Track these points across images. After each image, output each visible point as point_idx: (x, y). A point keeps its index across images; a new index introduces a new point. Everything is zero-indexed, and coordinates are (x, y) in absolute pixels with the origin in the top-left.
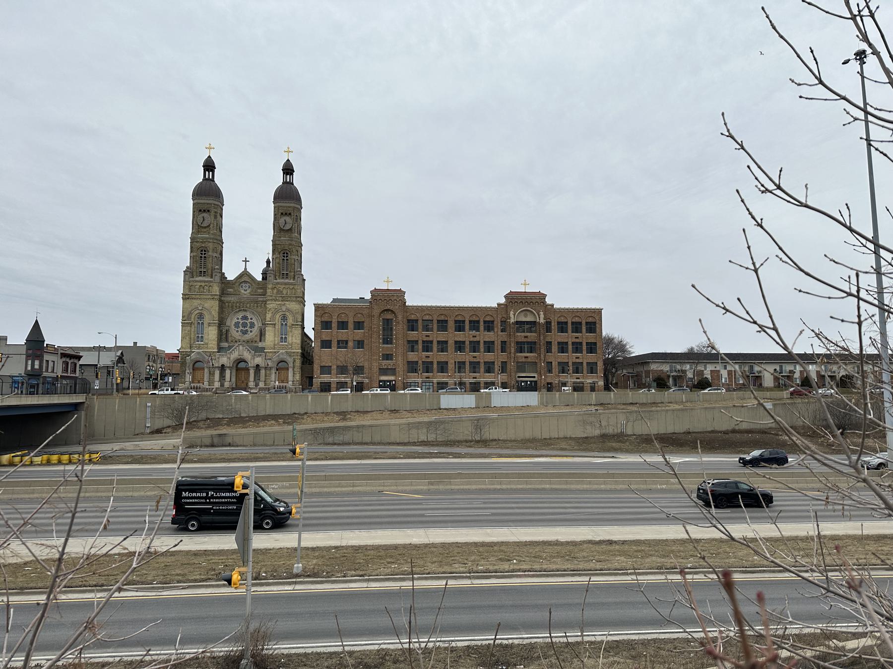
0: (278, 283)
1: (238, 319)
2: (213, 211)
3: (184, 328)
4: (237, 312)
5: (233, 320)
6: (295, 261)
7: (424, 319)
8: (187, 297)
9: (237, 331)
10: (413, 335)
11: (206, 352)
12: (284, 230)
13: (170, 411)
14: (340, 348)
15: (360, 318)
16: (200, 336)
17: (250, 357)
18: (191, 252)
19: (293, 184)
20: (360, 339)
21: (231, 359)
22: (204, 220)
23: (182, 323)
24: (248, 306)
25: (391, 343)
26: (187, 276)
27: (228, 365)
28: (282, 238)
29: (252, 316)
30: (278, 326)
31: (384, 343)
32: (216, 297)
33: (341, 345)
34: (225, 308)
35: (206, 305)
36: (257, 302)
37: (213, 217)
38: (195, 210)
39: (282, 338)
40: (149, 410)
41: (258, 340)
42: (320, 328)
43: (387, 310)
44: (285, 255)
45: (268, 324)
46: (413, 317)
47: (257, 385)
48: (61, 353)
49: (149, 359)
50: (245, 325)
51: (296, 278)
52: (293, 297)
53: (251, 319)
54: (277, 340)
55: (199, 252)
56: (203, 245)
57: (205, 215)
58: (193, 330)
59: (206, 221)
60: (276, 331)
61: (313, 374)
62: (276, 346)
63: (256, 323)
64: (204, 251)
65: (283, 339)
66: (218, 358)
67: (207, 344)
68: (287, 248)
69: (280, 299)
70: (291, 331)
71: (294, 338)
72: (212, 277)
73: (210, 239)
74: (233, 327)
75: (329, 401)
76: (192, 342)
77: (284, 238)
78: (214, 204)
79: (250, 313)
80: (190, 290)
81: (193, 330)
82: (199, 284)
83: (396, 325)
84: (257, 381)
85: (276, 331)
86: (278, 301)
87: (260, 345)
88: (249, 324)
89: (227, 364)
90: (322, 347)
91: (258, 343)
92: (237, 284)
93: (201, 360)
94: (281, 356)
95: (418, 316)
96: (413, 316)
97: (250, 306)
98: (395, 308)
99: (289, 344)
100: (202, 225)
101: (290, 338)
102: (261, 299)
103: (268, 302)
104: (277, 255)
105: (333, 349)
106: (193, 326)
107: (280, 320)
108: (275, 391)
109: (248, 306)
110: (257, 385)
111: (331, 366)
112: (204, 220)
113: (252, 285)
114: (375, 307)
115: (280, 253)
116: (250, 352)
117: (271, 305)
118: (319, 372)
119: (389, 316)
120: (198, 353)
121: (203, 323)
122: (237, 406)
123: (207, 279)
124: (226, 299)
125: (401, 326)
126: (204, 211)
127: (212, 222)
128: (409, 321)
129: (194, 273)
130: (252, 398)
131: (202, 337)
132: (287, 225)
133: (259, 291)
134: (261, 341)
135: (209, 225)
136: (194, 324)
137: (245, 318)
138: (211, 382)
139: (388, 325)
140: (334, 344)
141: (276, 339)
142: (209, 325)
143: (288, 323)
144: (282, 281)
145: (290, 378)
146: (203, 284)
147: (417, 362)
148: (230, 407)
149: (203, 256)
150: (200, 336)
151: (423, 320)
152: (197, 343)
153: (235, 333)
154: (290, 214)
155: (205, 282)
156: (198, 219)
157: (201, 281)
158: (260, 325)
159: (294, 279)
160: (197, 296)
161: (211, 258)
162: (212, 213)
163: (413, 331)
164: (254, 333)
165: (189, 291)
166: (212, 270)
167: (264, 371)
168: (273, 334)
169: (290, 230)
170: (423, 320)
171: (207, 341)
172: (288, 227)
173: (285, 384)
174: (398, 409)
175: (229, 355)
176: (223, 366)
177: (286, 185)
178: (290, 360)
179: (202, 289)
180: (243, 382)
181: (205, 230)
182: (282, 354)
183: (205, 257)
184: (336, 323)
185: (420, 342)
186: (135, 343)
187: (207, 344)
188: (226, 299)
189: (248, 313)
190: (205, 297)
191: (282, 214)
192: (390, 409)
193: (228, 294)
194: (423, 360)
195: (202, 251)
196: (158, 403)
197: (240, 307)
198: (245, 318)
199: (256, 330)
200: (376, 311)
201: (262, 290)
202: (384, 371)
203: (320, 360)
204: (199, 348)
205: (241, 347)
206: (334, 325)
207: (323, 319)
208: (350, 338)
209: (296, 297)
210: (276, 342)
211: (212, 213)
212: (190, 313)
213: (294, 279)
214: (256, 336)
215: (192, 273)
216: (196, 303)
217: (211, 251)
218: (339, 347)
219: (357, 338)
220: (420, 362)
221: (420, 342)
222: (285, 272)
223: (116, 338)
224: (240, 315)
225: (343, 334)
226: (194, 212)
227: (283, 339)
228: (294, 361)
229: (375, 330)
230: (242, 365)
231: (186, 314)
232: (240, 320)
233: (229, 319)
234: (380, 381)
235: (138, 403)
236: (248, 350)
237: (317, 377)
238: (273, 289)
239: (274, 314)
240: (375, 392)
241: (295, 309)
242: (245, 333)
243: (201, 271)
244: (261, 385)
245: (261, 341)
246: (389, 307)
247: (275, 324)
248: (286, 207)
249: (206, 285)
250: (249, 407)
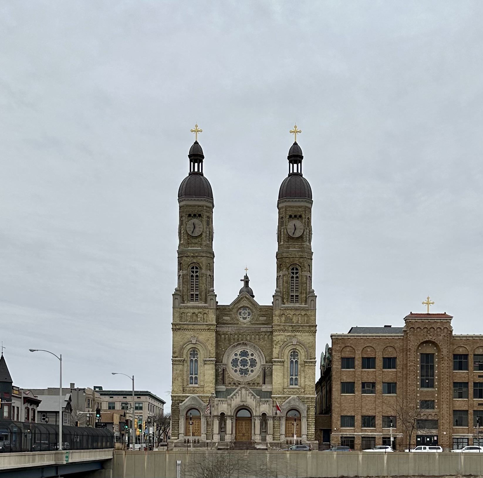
0: (287, 309)
1: (236, 355)
3: (175, 367)
4: (234, 346)
5: (228, 359)
6: (306, 279)
7: (476, 353)
8: (177, 327)
9: (252, 371)
10: (461, 375)
11: (202, 397)
12: (293, 238)
13: (200, 470)
14: (365, 393)
15: (390, 353)
16: (194, 376)
17: (255, 403)
18: (180, 269)
19: (202, 175)
20: (390, 381)
21: (232, 405)
22: (194, 228)
23: (173, 361)
24: (248, 338)
25: (432, 386)
27: (229, 414)
30: (287, 364)
31: (422, 386)
32: (212, 327)
33: (366, 388)
36: (259, 333)
37: (205, 223)
39: (292, 379)
40: (179, 468)
41: (261, 381)
42: (340, 367)
43: (426, 342)
44: (295, 271)
45: (275, 361)
46: (461, 351)
47: (264, 439)
48: (24, 397)
49: (89, 404)
50: (244, 363)
51: (209, 299)
52: (306, 326)
53: (252, 355)
54: (287, 381)
55: (190, 269)
56: (195, 261)
57: (196, 221)
59: (197, 229)
60: (285, 371)
61: (331, 426)
62: (285, 390)
64: (195, 267)
65: (294, 381)
66: (217, 405)
67: (203, 387)
69: (290, 329)
70: (304, 371)
71: (307, 380)
73: (203, 252)
74: (230, 365)
75: (385, 462)
76: (185, 384)
77: (294, 249)
78: (207, 207)
79: (250, 347)
80: (181, 318)
82: (192, 311)
83: (439, 362)
85: (285, 371)
86: (287, 331)
87: (266, 388)
88: (249, 361)
89: (228, 412)
90: (343, 391)
91: (261, 386)
92: (235, 310)
93: (197, 407)
94: (293, 403)
95: (469, 350)
96: (461, 350)
97: (251, 339)
98: (439, 339)
101: (303, 380)
102: (264, 330)
103: (275, 334)
104: (284, 272)
105: (356, 393)
106: (186, 365)
107: (289, 357)
109: (248, 338)
110: (264, 439)
111: (354, 416)
112: (194, 228)
114: (412, 338)
115: (288, 269)
116: (255, 398)
117: (279, 337)
119: (429, 350)
120: (193, 398)
121: (196, 361)
122: (273, 466)
123: (200, 305)
124: (224, 329)
125: (446, 362)
126: (195, 215)
128: (455, 356)
130: (290, 456)
131: (196, 378)
132: (297, 231)
133: (261, 318)
134: (265, 384)
135: (201, 234)
136: (186, 362)
137: (244, 354)
138: (210, 435)
139: (427, 362)
140: (358, 387)
141: (285, 380)
142: (205, 362)
143: (299, 361)
144: (292, 305)
145: (304, 431)
146: (196, 311)
147: (467, 411)
148: (265, 467)
149: (195, 274)
150: (194, 376)
151: (474, 355)
152: (190, 385)
153: (233, 374)
154: (300, 216)
155: (198, 308)
156: (188, 226)
157: (193, 307)
160: (190, 327)
163: (461, 369)
164: (255, 373)
165: (181, 320)
166: (206, 293)
167: (272, 421)
168: (282, 375)
169: (301, 237)
170: (474, 355)
171: (202, 384)
172: (298, 234)
173: (199, 437)
174: (475, 474)
175: (229, 401)
176: (223, 414)
177: (193, 176)
178: (303, 408)
179: (195, 318)
180: (244, 435)
181: (196, 241)
182: (294, 399)
184: (361, 360)
185: (471, 385)
186: (72, 385)
187: (203, 387)
188: (224, 329)
189: (248, 347)
190: (199, 327)
191: (290, 216)
192: (463, 474)
193: (224, 324)
194: (475, 409)
195: (193, 268)
196: (187, 461)
197: (238, 340)
198: (244, 354)
199: (258, 369)
200: (413, 343)
201: (265, 318)
202: (422, 423)
203: (340, 407)
204: (193, 392)
206: (358, 363)
207: (344, 355)
208: (378, 379)
209: (309, 326)
210: (286, 385)
211: (205, 219)
212: (182, 348)
214: (258, 377)
216: (189, 334)
217: (204, 268)
218: (364, 392)
219: (387, 380)
220: (471, 411)
221: (471, 385)
222: (294, 294)
223: (133, 380)
224: (239, 350)
225: (368, 375)
226: (181, 217)
227: (294, 381)
228: (308, 409)
229: (412, 368)
230: (244, 413)
231: (177, 350)
232: (238, 357)
234: (418, 436)
235: (167, 460)
236: (253, 395)
237: (337, 430)
239: (282, 348)
240: (423, 451)
242: (244, 372)
243: (192, 295)
244: (269, 439)
245: (265, 384)
246: (430, 338)
247: (283, 362)
248: (296, 207)
250: (287, 467)
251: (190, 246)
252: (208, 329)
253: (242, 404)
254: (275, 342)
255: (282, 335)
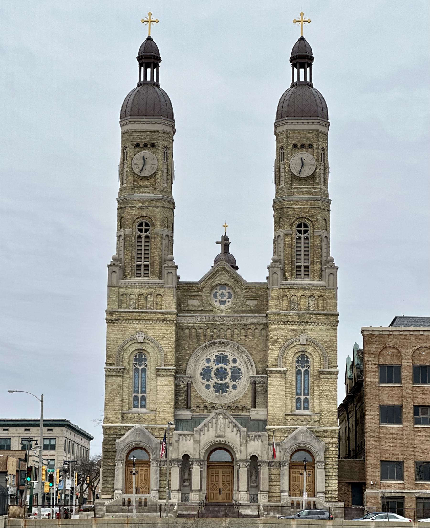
0: (290, 287)
1: (208, 361)
2: (161, 144)
3: (110, 380)
4: (206, 347)
8: (115, 317)
9: (234, 387)
11: (152, 428)
16: (140, 395)
18: (121, 225)
19: (158, 86)
21: (202, 442)
22: (303, 165)
23: (107, 370)
24: (228, 334)
26: (114, 276)
27: (197, 457)
28: (296, 195)
29: (237, 356)
30: (292, 376)
32: (170, 317)
33: (421, 416)
34: (184, 339)
35: (152, 334)
36: (245, 326)
37: (161, 157)
38: (128, 144)
39: (299, 400)
41: (248, 402)
42: (377, 380)
44: (303, 229)
45: (272, 371)
47: (254, 499)
50: (221, 374)
51: (165, 272)
52: (322, 315)
53: (235, 361)
54: (291, 403)
55: (136, 227)
56: (144, 214)
57: (146, 153)
58: (126, 383)
59: (148, 166)
60: (289, 386)
62: (288, 418)
63: (243, 369)
66: (177, 441)
67: (154, 412)
68: (306, 215)
69: (296, 319)
70: (318, 387)
72: (160, 277)
73: (157, 200)
74: (199, 378)
76: (126, 408)
79: (232, 347)
81: (126, 383)
82: (138, 291)
84: (186, 489)
85: (289, 386)
88: (229, 371)
89: (195, 454)
91: (249, 411)
92: (206, 290)
93: (144, 445)
94: (300, 439)
97: (232, 335)
99: (316, 414)
100: (143, 175)
101: (317, 401)
102: (254, 321)
103: (271, 327)
104: (286, 229)
105: (405, 423)
106: (127, 377)
107: (295, 364)
108: (309, 514)
109: (228, 334)
110: (254, 499)
111: (403, 462)
113: (235, 292)
115: (291, 225)
118: (378, 473)
120: (139, 431)
126: (145, 145)
127: (161, 166)
129: (128, 270)
131: (143, 398)
132: (306, 168)
133: (249, 303)
135: (155, 173)
137: (221, 359)
141: (289, 402)
143: (311, 371)
144: (298, 281)
146: (145, 291)
149: (143, 234)
150: (140, 395)
152: (134, 410)
154: (311, 146)
155: (148, 286)
156: (135, 161)
157: (141, 286)
158: (252, 373)
159: (321, 277)
160: (135, 316)
161: (158, 240)
162: (161, 150)
165: (120, 306)
166: (161, 263)
167: (267, 469)
168: (281, 393)
169: (312, 177)
171: (153, 407)
172: (307, 172)
175: (197, 436)
177: (144, 87)
179: (142, 302)
180: (220, 492)
181: (146, 183)
182: (303, 433)
183: (147, 237)
184: (411, 370)
187: (154, 412)
189: (228, 349)
190: (149, 316)
191: (295, 146)
193: (189, 311)
195: (141, 225)
197: (212, 337)
198: (221, 359)
201: (255, 302)
203: (379, 446)
204: (139, 421)
205: (220, 419)
207: (382, 361)
209: (327, 315)
210: (289, 409)
211: (161, 150)
212: (122, 350)
213: (321, 277)
214: (244, 396)
215: (123, 269)
217: (158, 224)
218: (417, 421)
222: (302, 264)
223: (42, 401)
228: (327, 449)
231: (113, 352)
232: (212, 364)
233: (191, 364)
236: (235, 426)
237: (374, 486)
238: (280, 298)
239: (284, 350)
241: (325, 339)
243: (139, 266)
245: (255, 407)
247: (285, 372)
248: (303, 132)
249: (151, 294)
251: (137, 191)
252: (164, 320)
253: (217, 440)
254: (272, 341)
255: (283, 329)
